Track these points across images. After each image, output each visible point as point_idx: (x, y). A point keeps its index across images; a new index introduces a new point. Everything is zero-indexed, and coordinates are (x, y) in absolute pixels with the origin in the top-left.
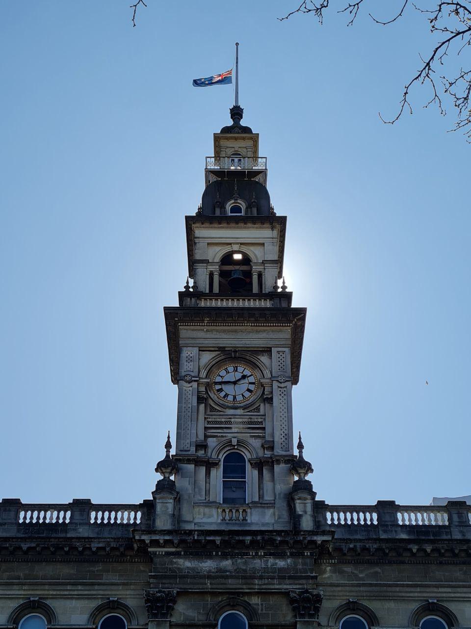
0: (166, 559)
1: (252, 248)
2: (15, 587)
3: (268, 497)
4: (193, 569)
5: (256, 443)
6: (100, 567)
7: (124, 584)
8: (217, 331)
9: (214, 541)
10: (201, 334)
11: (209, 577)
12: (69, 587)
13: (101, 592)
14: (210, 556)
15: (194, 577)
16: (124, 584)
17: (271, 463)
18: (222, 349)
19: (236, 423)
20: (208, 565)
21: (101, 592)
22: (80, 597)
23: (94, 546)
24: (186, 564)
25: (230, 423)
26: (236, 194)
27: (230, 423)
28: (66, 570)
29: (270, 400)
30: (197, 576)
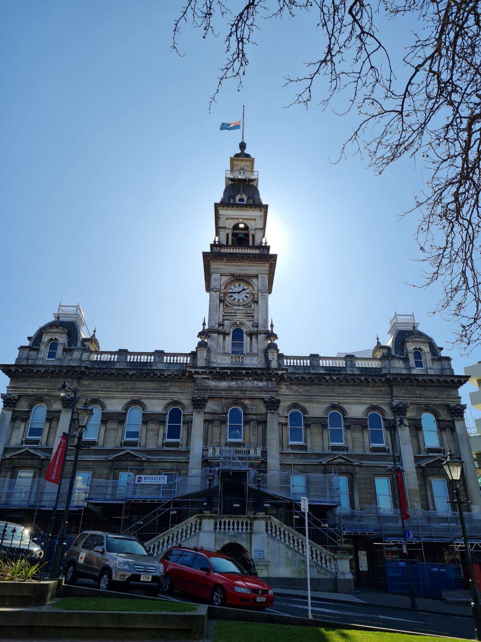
0: (203, 381)
1: (249, 221)
2: (126, 393)
3: (255, 351)
4: (216, 386)
5: (249, 324)
6: (169, 384)
7: (181, 392)
8: (230, 265)
9: (227, 373)
10: (221, 267)
11: (224, 390)
12: (153, 394)
13: (169, 396)
14: (225, 380)
15: (216, 390)
16: (181, 392)
17: (257, 334)
18: (232, 275)
19: (239, 313)
20: (224, 384)
21: (169, 396)
22: (158, 399)
23: (166, 374)
24: (212, 383)
25: (236, 313)
26: (241, 192)
27: (236, 313)
28: (152, 385)
29: (257, 302)
30: (217, 389)
